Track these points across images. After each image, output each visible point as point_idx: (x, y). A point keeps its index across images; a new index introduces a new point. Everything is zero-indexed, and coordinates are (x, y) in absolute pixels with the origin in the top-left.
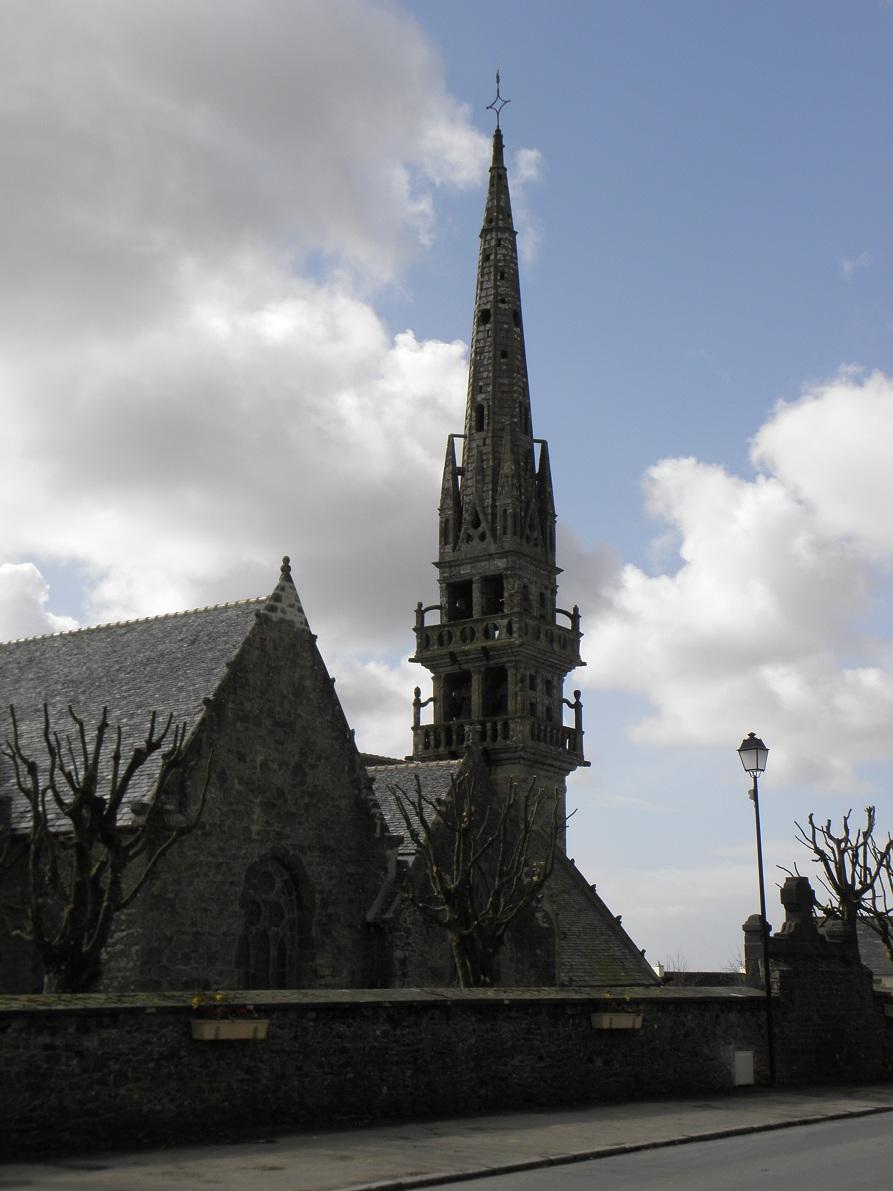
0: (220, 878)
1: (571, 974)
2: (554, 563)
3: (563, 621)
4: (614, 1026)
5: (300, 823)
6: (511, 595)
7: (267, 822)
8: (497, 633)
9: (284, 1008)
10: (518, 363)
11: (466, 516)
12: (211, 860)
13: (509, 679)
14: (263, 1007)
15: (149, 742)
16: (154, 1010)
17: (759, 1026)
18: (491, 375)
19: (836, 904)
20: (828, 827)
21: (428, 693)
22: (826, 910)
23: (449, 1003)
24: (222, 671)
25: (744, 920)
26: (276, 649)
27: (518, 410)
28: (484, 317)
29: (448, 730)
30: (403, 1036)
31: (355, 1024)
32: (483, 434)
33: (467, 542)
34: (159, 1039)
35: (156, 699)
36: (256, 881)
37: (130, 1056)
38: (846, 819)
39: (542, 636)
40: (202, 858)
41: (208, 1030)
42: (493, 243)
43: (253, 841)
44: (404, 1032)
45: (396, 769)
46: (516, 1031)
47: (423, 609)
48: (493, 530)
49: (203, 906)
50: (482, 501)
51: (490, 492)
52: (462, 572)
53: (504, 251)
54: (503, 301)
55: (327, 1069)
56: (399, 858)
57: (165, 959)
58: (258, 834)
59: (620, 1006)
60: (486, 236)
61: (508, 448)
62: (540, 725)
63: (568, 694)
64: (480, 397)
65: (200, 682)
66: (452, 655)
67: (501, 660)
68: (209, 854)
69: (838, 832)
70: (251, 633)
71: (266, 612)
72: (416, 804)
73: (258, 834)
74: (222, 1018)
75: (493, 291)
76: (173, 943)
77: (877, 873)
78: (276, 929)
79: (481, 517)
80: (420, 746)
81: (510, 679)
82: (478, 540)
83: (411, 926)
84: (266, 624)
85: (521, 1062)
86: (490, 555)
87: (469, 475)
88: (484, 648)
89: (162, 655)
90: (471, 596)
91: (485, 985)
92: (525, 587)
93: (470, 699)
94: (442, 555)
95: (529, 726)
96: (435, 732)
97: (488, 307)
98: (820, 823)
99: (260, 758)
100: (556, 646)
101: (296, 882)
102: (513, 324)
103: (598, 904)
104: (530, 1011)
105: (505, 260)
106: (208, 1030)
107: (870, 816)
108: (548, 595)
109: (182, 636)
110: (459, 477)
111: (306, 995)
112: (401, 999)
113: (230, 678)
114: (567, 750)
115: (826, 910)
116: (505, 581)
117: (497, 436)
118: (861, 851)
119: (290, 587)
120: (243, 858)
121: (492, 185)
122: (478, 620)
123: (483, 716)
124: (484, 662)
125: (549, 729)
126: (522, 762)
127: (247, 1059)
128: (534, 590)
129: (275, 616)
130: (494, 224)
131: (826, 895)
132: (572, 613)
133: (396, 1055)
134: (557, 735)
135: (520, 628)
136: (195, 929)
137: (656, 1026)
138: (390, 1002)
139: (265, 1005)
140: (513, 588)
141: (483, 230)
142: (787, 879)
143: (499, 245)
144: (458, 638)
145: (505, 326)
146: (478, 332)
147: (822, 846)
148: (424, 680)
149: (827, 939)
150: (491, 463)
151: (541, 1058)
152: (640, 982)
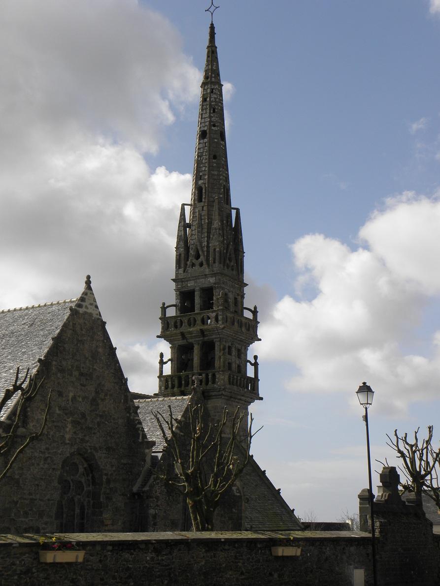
0: (46, 466)
1: (251, 524)
2: (243, 280)
3: (248, 315)
4: (285, 554)
5: (94, 433)
6: (218, 299)
7: (75, 433)
8: (209, 321)
9: (93, 544)
10: (223, 162)
11: (192, 252)
12: (41, 455)
13: (216, 348)
14: (81, 543)
15: (15, 386)
16: (18, 545)
17: (368, 554)
18: (207, 169)
19: (410, 483)
20: (406, 438)
21: (168, 356)
22: (404, 487)
23: (189, 541)
24: (49, 342)
25: (359, 492)
26: (82, 330)
27: (222, 190)
28: (203, 135)
29: (180, 378)
30: (163, 560)
31: (135, 553)
32: (202, 204)
33: (192, 267)
34: (20, 562)
35: (9, 359)
36: (68, 468)
37: (3, 572)
38: (416, 433)
39: (236, 323)
40: (36, 454)
41: (50, 557)
42: (209, 91)
43: (66, 444)
44: (163, 558)
45: (151, 401)
46: (228, 557)
47: (165, 306)
48: (207, 260)
49: (36, 483)
50: (201, 243)
51: (206, 238)
52: (189, 285)
53: (215, 96)
54: (214, 126)
55: (118, 580)
56: (153, 454)
57: (13, 515)
58: (69, 440)
59: (287, 542)
60: (204, 87)
61: (217, 213)
62: (234, 376)
63: (250, 357)
64: (200, 182)
65: (36, 350)
66: (183, 334)
67: (211, 337)
68: (40, 451)
69: (411, 441)
70: (67, 320)
71: (76, 308)
72: (169, 423)
73: (69, 440)
74: (57, 550)
75: (208, 120)
76: (18, 505)
77: (434, 466)
78: (79, 497)
79: (200, 253)
80: (163, 388)
81: (216, 348)
82: (199, 267)
83: (159, 495)
84: (76, 315)
85: (231, 575)
86: (205, 275)
87: (193, 228)
88: (201, 330)
89: (12, 333)
90: (194, 299)
91: (208, 530)
92: (226, 294)
93: (192, 360)
94: (177, 274)
95: (227, 376)
96: (172, 378)
97: (205, 129)
98: (401, 435)
99: (71, 395)
100: (244, 329)
101: (92, 468)
102: (220, 139)
103: (267, 482)
104: (236, 545)
105: (215, 101)
106: (50, 557)
107: (430, 431)
108: (239, 298)
109: (24, 321)
110: (188, 229)
111: (106, 536)
112: (161, 538)
113: (54, 347)
114: (249, 389)
115: (404, 487)
116: (214, 291)
117: (210, 205)
118: (425, 451)
119: (91, 294)
120: (60, 454)
121: (208, 57)
122: (197, 314)
123: (200, 370)
124: (201, 338)
125: (239, 378)
126: (223, 397)
127: (72, 574)
128: (231, 296)
129: (81, 310)
130: (209, 79)
131: (405, 478)
132: (253, 310)
133: (159, 571)
134: (244, 381)
135: (223, 318)
136: (31, 497)
137: (309, 554)
138: (155, 540)
139: (82, 542)
140: (219, 295)
141: (202, 83)
142: (384, 468)
143: (212, 92)
144: (186, 324)
145: (216, 140)
146: (199, 144)
147: (402, 448)
148: (165, 348)
149: (407, 503)
150: (207, 221)
151: (242, 573)
152: (292, 528)
